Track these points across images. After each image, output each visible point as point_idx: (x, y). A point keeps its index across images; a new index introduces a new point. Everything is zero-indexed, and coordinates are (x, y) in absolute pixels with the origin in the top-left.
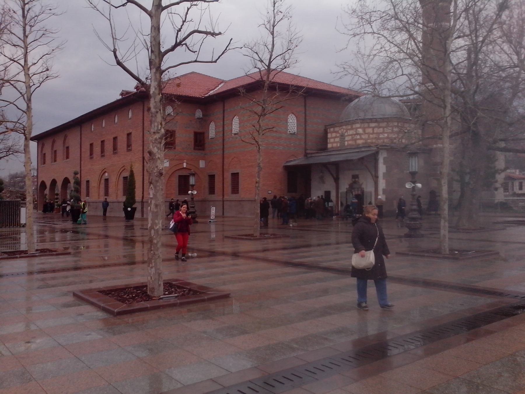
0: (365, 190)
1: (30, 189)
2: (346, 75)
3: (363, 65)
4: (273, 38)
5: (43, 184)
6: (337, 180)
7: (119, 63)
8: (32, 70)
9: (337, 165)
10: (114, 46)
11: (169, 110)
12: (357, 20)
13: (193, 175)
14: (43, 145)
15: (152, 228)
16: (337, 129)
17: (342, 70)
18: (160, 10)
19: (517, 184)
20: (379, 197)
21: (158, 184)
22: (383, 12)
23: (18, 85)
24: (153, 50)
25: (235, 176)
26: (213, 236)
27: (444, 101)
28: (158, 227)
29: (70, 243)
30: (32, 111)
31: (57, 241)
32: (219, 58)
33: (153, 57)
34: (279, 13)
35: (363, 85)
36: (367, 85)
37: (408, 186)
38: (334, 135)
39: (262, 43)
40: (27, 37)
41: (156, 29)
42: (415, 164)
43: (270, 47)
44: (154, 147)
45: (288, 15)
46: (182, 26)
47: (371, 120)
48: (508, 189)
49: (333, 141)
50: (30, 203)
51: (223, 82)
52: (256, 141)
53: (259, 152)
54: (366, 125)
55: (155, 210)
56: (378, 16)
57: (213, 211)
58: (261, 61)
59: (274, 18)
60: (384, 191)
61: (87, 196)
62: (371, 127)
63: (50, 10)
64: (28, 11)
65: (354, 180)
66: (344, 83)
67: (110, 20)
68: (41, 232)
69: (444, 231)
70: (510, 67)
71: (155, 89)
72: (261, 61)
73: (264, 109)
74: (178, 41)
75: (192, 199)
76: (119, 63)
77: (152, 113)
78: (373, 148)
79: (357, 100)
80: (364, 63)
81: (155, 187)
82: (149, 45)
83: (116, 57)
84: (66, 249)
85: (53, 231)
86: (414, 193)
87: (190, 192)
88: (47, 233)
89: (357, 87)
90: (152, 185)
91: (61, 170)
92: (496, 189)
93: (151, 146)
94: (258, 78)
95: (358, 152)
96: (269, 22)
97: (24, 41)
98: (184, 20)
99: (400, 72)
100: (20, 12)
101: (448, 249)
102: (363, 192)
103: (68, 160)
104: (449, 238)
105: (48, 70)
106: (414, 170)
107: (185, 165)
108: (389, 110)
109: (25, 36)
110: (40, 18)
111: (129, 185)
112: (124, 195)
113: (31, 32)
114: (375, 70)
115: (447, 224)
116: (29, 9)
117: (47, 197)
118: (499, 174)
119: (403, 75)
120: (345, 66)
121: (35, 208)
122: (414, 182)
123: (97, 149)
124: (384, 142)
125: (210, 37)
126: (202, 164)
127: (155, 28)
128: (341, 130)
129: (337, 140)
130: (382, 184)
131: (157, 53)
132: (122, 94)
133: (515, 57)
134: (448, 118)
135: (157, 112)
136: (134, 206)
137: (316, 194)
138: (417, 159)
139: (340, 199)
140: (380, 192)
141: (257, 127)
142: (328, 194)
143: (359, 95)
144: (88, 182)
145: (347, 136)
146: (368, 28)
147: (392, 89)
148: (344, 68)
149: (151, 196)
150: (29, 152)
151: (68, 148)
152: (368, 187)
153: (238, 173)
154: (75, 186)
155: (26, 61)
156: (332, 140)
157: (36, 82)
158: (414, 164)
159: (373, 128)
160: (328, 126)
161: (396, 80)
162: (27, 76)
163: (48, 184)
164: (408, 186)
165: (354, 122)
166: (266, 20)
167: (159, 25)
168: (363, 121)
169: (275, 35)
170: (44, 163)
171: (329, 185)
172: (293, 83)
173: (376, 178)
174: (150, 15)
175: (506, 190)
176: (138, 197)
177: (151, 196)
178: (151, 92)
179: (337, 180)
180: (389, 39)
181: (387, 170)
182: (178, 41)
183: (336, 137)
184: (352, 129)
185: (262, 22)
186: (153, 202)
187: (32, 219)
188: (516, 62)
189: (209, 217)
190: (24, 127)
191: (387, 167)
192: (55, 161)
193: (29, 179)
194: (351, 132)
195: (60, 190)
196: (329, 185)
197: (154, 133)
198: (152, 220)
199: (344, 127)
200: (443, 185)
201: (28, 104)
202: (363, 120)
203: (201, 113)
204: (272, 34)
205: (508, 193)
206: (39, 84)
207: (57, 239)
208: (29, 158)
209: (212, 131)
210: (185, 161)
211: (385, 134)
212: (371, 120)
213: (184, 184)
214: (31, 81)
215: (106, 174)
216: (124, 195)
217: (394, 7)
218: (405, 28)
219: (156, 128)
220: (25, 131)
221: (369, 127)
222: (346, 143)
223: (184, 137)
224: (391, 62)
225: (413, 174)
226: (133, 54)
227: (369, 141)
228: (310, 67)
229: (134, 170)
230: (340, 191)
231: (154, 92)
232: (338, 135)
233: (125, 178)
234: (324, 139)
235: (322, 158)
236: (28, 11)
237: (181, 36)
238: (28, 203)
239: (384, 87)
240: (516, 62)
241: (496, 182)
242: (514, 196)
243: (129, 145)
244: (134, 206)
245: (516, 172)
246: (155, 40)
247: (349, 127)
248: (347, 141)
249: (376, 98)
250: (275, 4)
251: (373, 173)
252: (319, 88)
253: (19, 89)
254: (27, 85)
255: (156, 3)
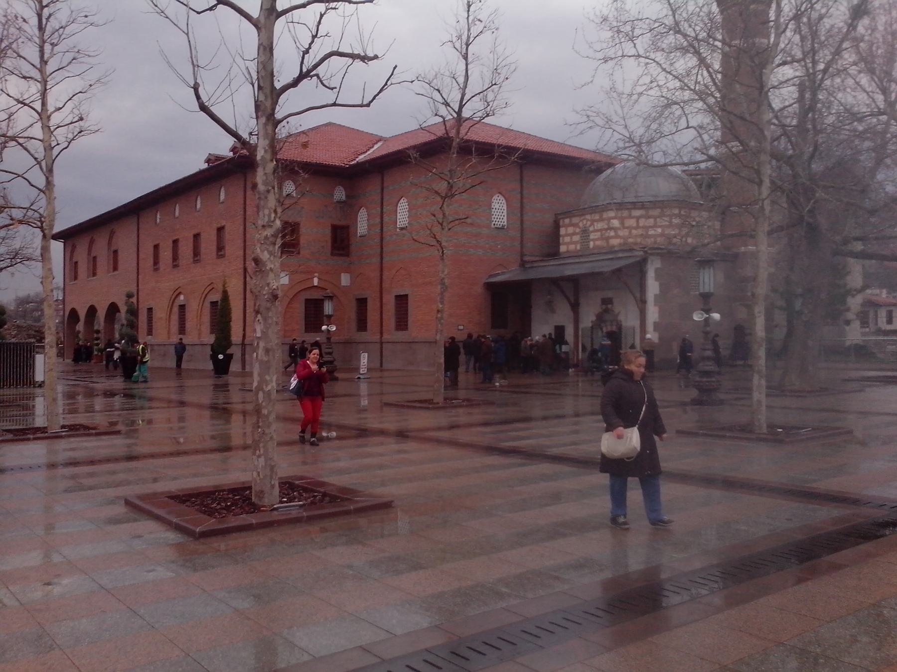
0: (624, 324)
1: (52, 323)
2: (591, 127)
3: (620, 112)
4: (467, 65)
5: (74, 314)
6: (575, 307)
7: (203, 108)
8: (55, 119)
9: (575, 281)
10: (195, 79)
11: (289, 187)
12: (609, 34)
13: (330, 298)
14: (74, 247)
15: (259, 388)
16: (575, 220)
17: (585, 119)
18: (273, 17)
19: (883, 314)
20: (648, 336)
21: (270, 314)
22: (655, 21)
23: (31, 145)
24: (262, 85)
25: (402, 301)
26: (364, 402)
27: (758, 172)
28: (269, 388)
29: (119, 415)
30: (55, 189)
31: (98, 412)
32: (374, 98)
33: (262, 98)
34: (477, 22)
35: (621, 144)
36: (627, 145)
37: (697, 317)
38: (571, 230)
39: (447, 73)
40: (46, 63)
41: (267, 49)
42: (709, 280)
43: (461, 80)
44: (262, 251)
45: (493, 26)
46: (310, 44)
47: (635, 205)
48: (867, 323)
49: (569, 241)
50: (51, 347)
51: (380, 139)
52: (438, 241)
53: (442, 259)
54: (626, 213)
55: (265, 359)
56: (645, 26)
57: (364, 359)
58: (447, 104)
59: (469, 30)
60: (657, 326)
61: (148, 335)
62: (633, 217)
63: (86, 16)
64: (48, 19)
65: (604, 307)
66: (589, 142)
67: (187, 34)
68: (70, 396)
69: (759, 394)
70: (872, 115)
71: (266, 151)
72: (447, 104)
73: (451, 187)
74: (304, 70)
75: (329, 339)
76: (203, 108)
77: (259, 193)
78: (637, 253)
79: (609, 171)
80: (622, 107)
81: (265, 319)
82: (255, 76)
83: (198, 97)
84: (113, 424)
85: (90, 394)
86: (708, 329)
87: (324, 327)
88: (80, 397)
89: (610, 149)
90: (259, 316)
91: (104, 290)
92: (848, 322)
93: (258, 250)
94: (440, 132)
95: (612, 259)
96: (459, 37)
97: (41, 71)
98: (314, 34)
99: (683, 123)
100: (34, 21)
101: (765, 425)
102: (620, 328)
103: (116, 273)
104: (767, 406)
105: (81, 119)
106: (707, 290)
107: (316, 282)
108: (664, 188)
109: (44, 62)
110: (68, 30)
111: (221, 315)
112: (211, 333)
113: (52, 55)
114: (641, 120)
115: (763, 382)
116: (50, 15)
117: (81, 336)
118: (853, 296)
119: (688, 127)
120: (590, 113)
121: (61, 354)
122: (708, 311)
123: (166, 254)
124: (655, 242)
125: (358, 63)
126: (345, 280)
127: (265, 49)
128: (583, 222)
129: (576, 238)
130: (653, 314)
131: (268, 91)
132: (208, 161)
133: (880, 98)
134: (766, 202)
135: (268, 191)
136: (229, 352)
137: (540, 331)
138: (712, 271)
139: (580, 339)
140: (650, 327)
141: (440, 217)
142: (560, 330)
143: (613, 161)
144: (150, 310)
145: (592, 232)
146: (629, 48)
147: (670, 152)
148: (588, 116)
149: (259, 335)
150: (50, 259)
151: (116, 252)
152: (629, 319)
153: (407, 295)
154: (129, 317)
155: (44, 104)
156: (567, 239)
157: (61, 139)
158: (707, 280)
159: (638, 218)
160: (560, 214)
161: (676, 137)
162: (47, 129)
163: (82, 314)
164: (697, 317)
165: (605, 208)
166: (455, 35)
167: (272, 43)
168: (621, 206)
169: (470, 60)
170: (76, 278)
171: (562, 316)
172: (500, 142)
173: (642, 303)
174: (256, 26)
175: (864, 323)
176: (236, 336)
177: (259, 335)
178: (258, 158)
179: (575, 307)
180: (664, 66)
181: (660, 291)
182: (304, 70)
183: (574, 234)
184: (601, 220)
185: (448, 38)
186: (262, 344)
187: (55, 374)
188: (882, 106)
189: (357, 369)
190: (41, 216)
191: (661, 285)
192: (94, 274)
193: (50, 306)
194: (599, 226)
195: (102, 323)
196: (562, 316)
197: (263, 226)
198: (259, 375)
199: (588, 217)
200: (757, 315)
201: (47, 178)
202: (620, 204)
203: (344, 193)
204: (466, 57)
205: (867, 330)
206: (66, 144)
207: (97, 408)
208: (50, 269)
209: (362, 224)
210: (316, 274)
211: (657, 229)
212: (635, 205)
213: (314, 314)
214: (53, 138)
215: (182, 297)
216: (211, 333)
217: (674, 12)
218: (692, 47)
219: (266, 219)
220: (42, 223)
221: (630, 217)
222: (591, 244)
223: (314, 234)
224: (668, 106)
225: (706, 297)
226: (228, 93)
227: (630, 240)
228: (529, 114)
229: (229, 289)
230: (581, 326)
231: (262, 157)
232: (578, 230)
233: (214, 304)
234: (554, 237)
235: (550, 269)
236: (48, 19)
237: (310, 61)
238: (47, 347)
239: (657, 149)
240: (882, 106)
241: (848, 310)
242: (879, 335)
243: (220, 248)
244: (229, 352)
245: (881, 293)
246: (264, 67)
247: (597, 217)
248: (594, 240)
249: (642, 167)
250: (469, 6)
251: (638, 295)
252: (546, 150)
253: (33, 152)
254: (47, 144)
255: (267, 5)
